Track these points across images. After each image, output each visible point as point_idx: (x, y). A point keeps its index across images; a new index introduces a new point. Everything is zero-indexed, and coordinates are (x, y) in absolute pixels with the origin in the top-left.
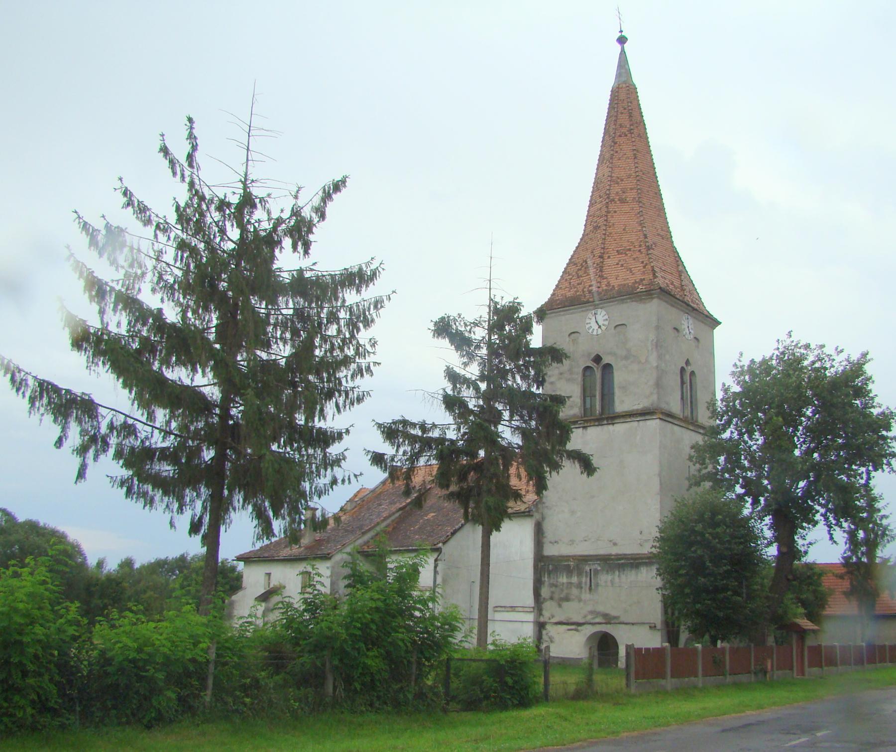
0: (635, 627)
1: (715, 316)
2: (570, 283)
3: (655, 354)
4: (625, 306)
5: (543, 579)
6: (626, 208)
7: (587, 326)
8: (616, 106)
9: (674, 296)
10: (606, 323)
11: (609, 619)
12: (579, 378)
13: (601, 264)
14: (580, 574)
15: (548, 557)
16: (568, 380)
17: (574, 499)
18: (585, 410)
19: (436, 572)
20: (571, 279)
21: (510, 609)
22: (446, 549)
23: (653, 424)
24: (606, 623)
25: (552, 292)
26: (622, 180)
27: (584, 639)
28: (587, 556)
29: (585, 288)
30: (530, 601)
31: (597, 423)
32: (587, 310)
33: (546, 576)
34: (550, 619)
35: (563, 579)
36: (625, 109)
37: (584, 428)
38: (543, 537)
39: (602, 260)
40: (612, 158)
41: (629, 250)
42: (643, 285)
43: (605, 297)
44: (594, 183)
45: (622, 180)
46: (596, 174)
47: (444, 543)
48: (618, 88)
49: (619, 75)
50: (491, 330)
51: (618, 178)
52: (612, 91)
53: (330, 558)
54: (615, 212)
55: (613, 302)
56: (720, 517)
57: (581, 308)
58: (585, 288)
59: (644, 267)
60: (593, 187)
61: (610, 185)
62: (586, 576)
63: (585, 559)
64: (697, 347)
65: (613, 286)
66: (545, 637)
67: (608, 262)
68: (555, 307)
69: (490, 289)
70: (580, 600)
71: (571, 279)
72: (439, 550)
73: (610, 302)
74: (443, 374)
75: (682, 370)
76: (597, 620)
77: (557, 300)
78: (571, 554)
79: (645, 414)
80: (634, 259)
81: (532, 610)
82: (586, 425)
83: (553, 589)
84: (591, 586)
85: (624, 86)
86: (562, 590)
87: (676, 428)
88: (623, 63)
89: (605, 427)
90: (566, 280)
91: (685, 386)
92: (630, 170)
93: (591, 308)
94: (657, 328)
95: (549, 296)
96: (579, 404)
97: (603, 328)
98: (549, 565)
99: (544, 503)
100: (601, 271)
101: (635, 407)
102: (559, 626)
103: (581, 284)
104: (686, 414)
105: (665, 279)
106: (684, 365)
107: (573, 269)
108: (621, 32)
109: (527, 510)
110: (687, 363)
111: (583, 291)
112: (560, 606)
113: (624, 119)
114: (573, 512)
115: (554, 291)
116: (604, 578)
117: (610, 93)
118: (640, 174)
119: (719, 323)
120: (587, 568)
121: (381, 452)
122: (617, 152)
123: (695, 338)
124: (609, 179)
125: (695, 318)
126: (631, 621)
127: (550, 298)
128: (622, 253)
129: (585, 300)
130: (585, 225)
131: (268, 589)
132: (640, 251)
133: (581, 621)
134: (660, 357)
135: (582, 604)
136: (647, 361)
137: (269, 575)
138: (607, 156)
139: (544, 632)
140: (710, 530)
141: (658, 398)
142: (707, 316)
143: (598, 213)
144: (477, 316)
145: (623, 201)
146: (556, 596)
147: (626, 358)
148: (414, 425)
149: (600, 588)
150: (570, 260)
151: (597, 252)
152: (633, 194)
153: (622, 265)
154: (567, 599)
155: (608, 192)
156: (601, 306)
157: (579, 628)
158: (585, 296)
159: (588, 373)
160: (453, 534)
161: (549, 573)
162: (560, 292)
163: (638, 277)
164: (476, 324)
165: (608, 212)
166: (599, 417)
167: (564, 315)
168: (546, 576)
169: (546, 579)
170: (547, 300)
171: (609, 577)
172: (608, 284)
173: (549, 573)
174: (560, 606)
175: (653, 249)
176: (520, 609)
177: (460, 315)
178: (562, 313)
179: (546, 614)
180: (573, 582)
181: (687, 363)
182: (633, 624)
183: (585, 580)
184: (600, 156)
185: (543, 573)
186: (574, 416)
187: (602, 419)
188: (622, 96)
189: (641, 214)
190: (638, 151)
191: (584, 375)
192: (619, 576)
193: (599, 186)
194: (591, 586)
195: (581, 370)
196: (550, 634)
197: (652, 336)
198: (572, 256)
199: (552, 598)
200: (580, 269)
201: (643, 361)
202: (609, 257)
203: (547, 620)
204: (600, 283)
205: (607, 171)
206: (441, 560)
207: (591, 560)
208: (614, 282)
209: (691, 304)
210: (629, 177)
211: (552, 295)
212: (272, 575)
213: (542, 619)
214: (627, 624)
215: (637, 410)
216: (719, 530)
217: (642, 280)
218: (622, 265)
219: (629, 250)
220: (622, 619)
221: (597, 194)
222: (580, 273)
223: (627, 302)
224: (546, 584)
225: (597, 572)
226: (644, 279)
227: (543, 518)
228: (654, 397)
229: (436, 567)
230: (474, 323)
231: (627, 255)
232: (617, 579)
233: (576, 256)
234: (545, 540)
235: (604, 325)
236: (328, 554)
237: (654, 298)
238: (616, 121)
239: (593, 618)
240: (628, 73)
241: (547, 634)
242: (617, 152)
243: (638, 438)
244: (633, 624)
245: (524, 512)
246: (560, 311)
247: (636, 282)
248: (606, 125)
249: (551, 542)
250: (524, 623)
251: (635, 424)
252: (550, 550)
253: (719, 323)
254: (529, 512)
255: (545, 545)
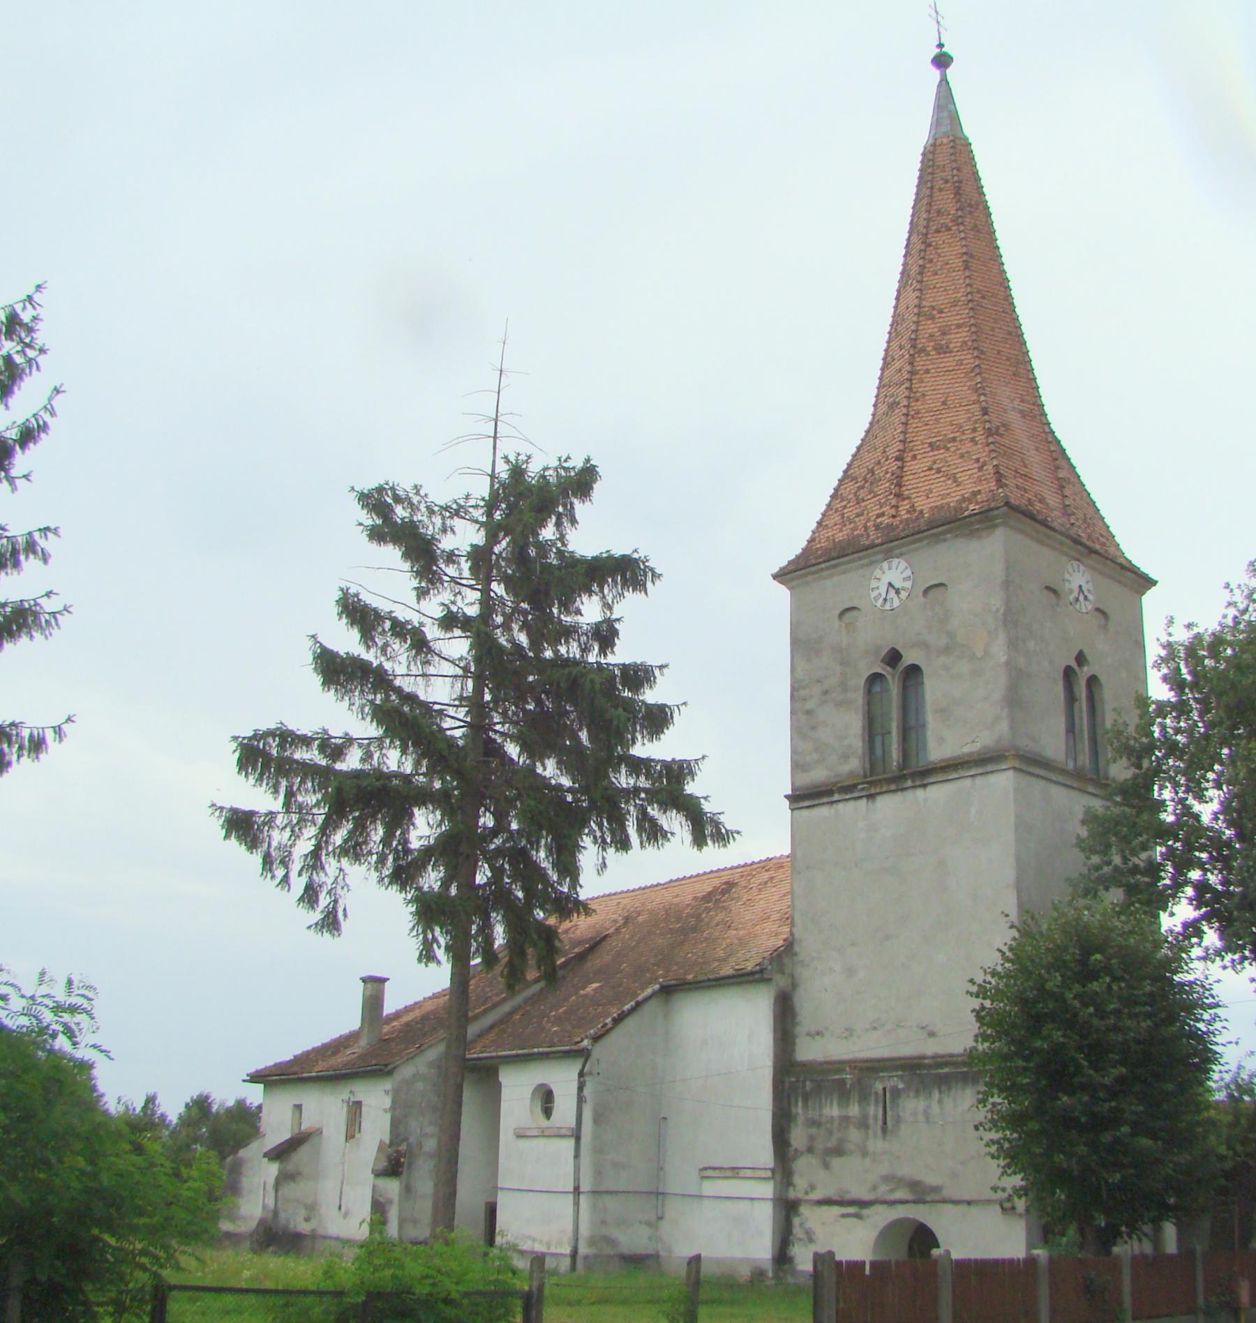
0: (974, 1210)
1: (1145, 568)
2: (843, 514)
3: (1002, 637)
4: (941, 547)
5: (794, 1110)
6: (949, 361)
7: (873, 594)
8: (930, 178)
9: (1044, 523)
10: (908, 584)
11: (921, 1193)
12: (859, 697)
13: (898, 472)
14: (863, 1099)
15: (804, 1065)
16: (839, 704)
17: (853, 944)
18: (872, 765)
19: (581, 1100)
20: (845, 507)
21: (729, 1173)
22: (598, 1051)
23: (1003, 781)
24: (914, 1202)
25: (808, 535)
26: (941, 312)
27: (874, 1234)
28: (879, 1060)
29: (869, 520)
30: (765, 1155)
31: (893, 787)
32: (872, 563)
33: (800, 1104)
34: (807, 1193)
35: (833, 1110)
36: (947, 182)
37: (871, 797)
38: (795, 1024)
39: (899, 464)
40: (921, 273)
41: (954, 440)
42: (977, 503)
43: (903, 535)
44: (892, 325)
45: (941, 312)
46: (896, 307)
47: (596, 1039)
48: (934, 145)
49: (937, 123)
50: (493, 531)
51: (933, 308)
52: (924, 154)
53: (390, 1073)
54: (927, 371)
55: (920, 540)
56: (1098, 956)
57: (860, 559)
58: (869, 520)
59: (980, 469)
60: (890, 333)
61: (917, 323)
62: (877, 1102)
63: (872, 1067)
64: (1105, 628)
65: (921, 512)
66: (797, 1231)
67: (911, 466)
68: (813, 562)
69: (495, 438)
70: (864, 1153)
71: (845, 507)
72: (585, 1054)
73: (913, 542)
74: (335, 610)
75: (1068, 673)
76: (899, 1195)
77: (817, 549)
78: (846, 1057)
79: (983, 761)
80: (962, 456)
81: (769, 1174)
82: (873, 791)
83: (814, 1131)
84: (885, 1123)
85: (945, 141)
86: (830, 1133)
87: (1055, 790)
88: (945, 101)
89: (909, 794)
90: (836, 511)
91: (1077, 705)
92: (956, 291)
93: (880, 556)
94: (1007, 584)
95: (804, 544)
96: (860, 752)
97: (904, 595)
98: (804, 1082)
99: (796, 954)
100: (899, 485)
101: (966, 750)
102: (825, 1208)
103: (862, 514)
104: (1079, 763)
105: (1025, 491)
106: (1074, 665)
107: (851, 486)
108: (940, 46)
109: (758, 968)
110: (1081, 659)
111: (866, 528)
112: (826, 1166)
113: (946, 201)
114: (850, 972)
115: (814, 532)
116: (911, 1106)
117: (920, 158)
118: (977, 297)
119: (1153, 583)
120: (879, 1086)
121: (247, 809)
122: (931, 261)
123: (1098, 610)
124: (916, 310)
125: (1095, 569)
126: (966, 1197)
127: (807, 547)
128: (938, 448)
129: (867, 543)
130: (875, 406)
131: (297, 1132)
132: (972, 440)
133: (867, 1197)
134: (1014, 644)
135: (867, 1161)
136: (987, 653)
137: (298, 1107)
138: (914, 270)
139: (796, 1221)
140: (1077, 988)
141: (1011, 728)
142: (1122, 567)
143: (896, 378)
144: (459, 495)
145: (942, 350)
146: (820, 1145)
147: (947, 650)
148: (306, 741)
149: (903, 1126)
150: (845, 472)
151: (893, 451)
152: (963, 335)
153: (939, 471)
154: (839, 1151)
155: (913, 336)
156: (897, 552)
157: (865, 1212)
158: (868, 536)
159: (877, 688)
160: (617, 1021)
161: (806, 1098)
162: (824, 534)
163: (968, 488)
164: (458, 511)
165: (912, 373)
166: (897, 774)
167: (832, 576)
168: (800, 1104)
169: (800, 1111)
170: (799, 551)
171: (921, 1104)
172: (912, 509)
173: (806, 1098)
174: (826, 1166)
175: (1001, 436)
176: (749, 1173)
177: (417, 489)
178: (825, 573)
179: (800, 1182)
180: (851, 1114)
181: (1081, 659)
182: (969, 1203)
183: (874, 1110)
184: (902, 273)
185: (793, 1100)
186: (851, 773)
187: (903, 777)
188: (942, 159)
189: (977, 370)
190: (971, 256)
191: (869, 692)
192: (940, 1101)
193: (899, 328)
194: (885, 1123)
195: (861, 682)
196: (807, 1226)
197: (997, 601)
198: (850, 465)
199: (810, 1150)
200: (863, 487)
201: (979, 654)
202: (914, 457)
203: (800, 1195)
204: (897, 507)
205: (911, 297)
206: (590, 1073)
207: (885, 1069)
208: (923, 504)
209: (1085, 541)
210: (955, 303)
211: (809, 542)
212: (303, 1107)
213: (792, 1194)
214: (956, 1202)
215: (971, 754)
216: (1095, 986)
217: (975, 494)
218: (939, 471)
219: (954, 440)
220: (947, 1193)
221: (895, 345)
222: (862, 494)
223: (945, 540)
224: (801, 1119)
225: (896, 1093)
226: (979, 492)
227: (794, 985)
228: (1004, 726)
229: (581, 1088)
230: (447, 508)
231: (947, 449)
232: (935, 1108)
233: (856, 464)
234: (800, 1030)
235: (903, 589)
236: (386, 1065)
237: (996, 526)
238: (929, 204)
239: (892, 1191)
240: (954, 119)
241: (801, 1224)
242: (931, 261)
243: (973, 811)
244: (969, 1203)
245: (752, 973)
246: (822, 570)
247: (964, 499)
248: (913, 215)
249: (809, 1034)
250: (756, 1203)
251: (968, 782)
252: (808, 1051)
253: (1153, 583)
254: (761, 971)
255: (798, 1041)
